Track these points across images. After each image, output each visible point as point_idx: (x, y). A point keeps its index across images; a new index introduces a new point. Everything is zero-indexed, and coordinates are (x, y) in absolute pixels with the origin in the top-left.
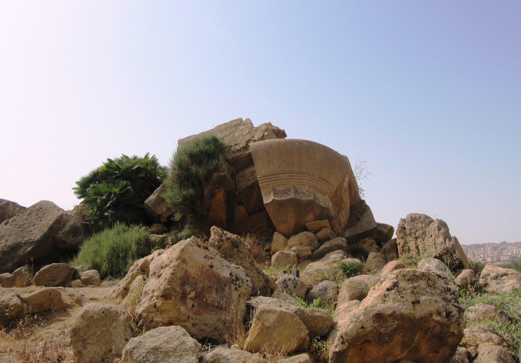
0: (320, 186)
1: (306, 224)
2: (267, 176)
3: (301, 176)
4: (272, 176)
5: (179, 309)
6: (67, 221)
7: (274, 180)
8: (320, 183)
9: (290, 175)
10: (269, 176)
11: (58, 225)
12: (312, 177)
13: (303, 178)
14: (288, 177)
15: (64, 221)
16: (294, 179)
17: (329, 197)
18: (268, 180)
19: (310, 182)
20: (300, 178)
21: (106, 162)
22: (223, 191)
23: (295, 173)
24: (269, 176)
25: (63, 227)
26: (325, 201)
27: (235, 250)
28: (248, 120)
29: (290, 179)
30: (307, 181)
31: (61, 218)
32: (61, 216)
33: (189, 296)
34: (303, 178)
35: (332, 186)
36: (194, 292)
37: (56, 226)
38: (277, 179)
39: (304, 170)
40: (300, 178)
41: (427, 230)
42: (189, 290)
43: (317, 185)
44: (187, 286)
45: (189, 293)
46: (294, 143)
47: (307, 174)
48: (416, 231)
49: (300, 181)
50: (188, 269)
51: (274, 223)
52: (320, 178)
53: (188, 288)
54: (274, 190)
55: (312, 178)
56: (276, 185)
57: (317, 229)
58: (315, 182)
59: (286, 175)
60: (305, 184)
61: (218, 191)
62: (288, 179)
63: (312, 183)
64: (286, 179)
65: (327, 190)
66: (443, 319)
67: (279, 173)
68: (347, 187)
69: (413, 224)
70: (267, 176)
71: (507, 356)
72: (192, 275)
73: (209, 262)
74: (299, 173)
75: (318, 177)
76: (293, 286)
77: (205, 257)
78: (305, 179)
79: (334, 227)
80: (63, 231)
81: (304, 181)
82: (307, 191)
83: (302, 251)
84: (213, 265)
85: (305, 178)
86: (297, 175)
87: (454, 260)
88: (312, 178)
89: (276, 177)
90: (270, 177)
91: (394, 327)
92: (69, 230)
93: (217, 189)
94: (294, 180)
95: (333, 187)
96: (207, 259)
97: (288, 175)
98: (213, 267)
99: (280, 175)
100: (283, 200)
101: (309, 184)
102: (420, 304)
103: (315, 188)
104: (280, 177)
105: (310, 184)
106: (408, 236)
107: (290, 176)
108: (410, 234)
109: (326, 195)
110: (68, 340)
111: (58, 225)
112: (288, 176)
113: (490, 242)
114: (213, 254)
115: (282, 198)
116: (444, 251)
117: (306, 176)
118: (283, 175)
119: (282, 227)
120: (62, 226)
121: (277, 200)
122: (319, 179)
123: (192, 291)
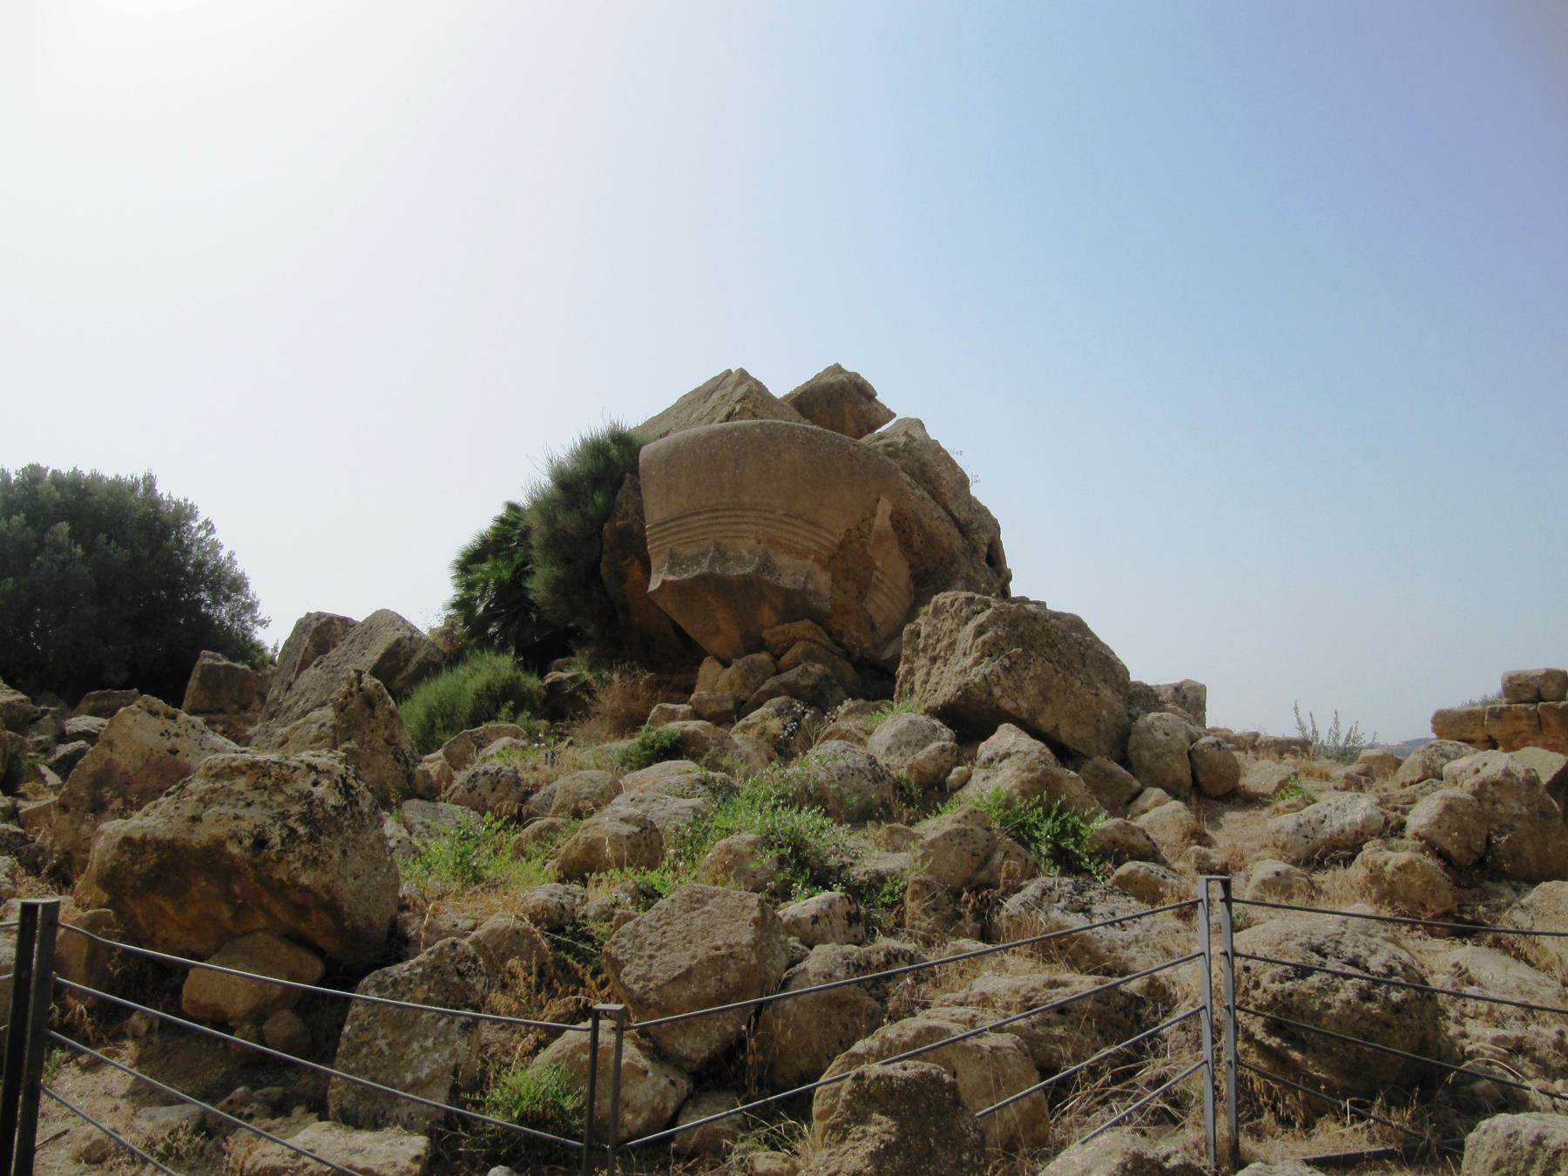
1: (765, 634)
2: (673, 520)
3: (736, 516)
4: (673, 524)
5: (78, 829)
6: (414, 651)
7: (675, 533)
8: (790, 528)
9: (712, 515)
10: (666, 522)
11: (394, 662)
12: (767, 515)
13: (741, 520)
14: (706, 522)
15: (406, 653)
16: (720, 524)
17: (818, 560)
18: (666, 533)
19: (761, 527)
20: (733, 520)
21: (500, 511)
22: (636, 563)
23: (724, 510)
24: (666, 522)
25: (406, 665)
26: (791, 571)
27: (368, 711)
29: (712, 525)
31: (399, 645)
32: (398, 643)
33: (111, 807)
34: (741, 520)
35: (827, 530)
36: (120, 799)
37: (387, 664)
39: (746, 499)
40: (733, 520)
41: (960, 636)
42: (109, 795)
44: (105, 789)
45: (110, 802)
46: (728, 433)
47: (752, 509)
48: (938, 641)
49: (734, 527)
50: (116, 757)
51: (695, 636)
53: (107, 792)
54: (671, 558)
55: (765, 519)
56: (679, 545)
57: (785, 644)
58: (773, 527)
59: (702, 517)
60: (743, 534)
61: (628, 565)
62: (707, 526)
63: (766, 529)
64: (702, 526)
68: (890, 529)
69: (934, 621)
70: (673, 520)
72: (123, 766)
73: (168, 745)
74: (733, 509)
75: (781, 512)
76: (489, 787)
77: (162, 735)
78: (746, 523)
79: (841, 635)
80: (405, 674)
81: (744, 526)
82: (750, 552)
83: (707, 702)
84: (179, 748)
85: (746, 520)
86: (727, 513)
88: (765, 519)
89: (679, 526)
90: (668, 525)
91: (152, 862)
92: (414, 672)
93: (624, 559)
95: (833, 534)
96: (167, 737)
97: (707, 515)
98: (178, 751)
99: (689, 519)
100: (684, 580)
103: (772, 541)
106: (921, 654)
107: (712, 518)
108: (925, 650)
109: (806, 558)
111: (394, 662)
112: (708, 519)
114: (184, 727)
115: (685, 576)
116: (960, 693)
117: (749, 513)
118: (696, 518)
119: (716, 644)
120: (402, 664)
121: (671, 581)
122: (787, 520)
123: (116, 798)
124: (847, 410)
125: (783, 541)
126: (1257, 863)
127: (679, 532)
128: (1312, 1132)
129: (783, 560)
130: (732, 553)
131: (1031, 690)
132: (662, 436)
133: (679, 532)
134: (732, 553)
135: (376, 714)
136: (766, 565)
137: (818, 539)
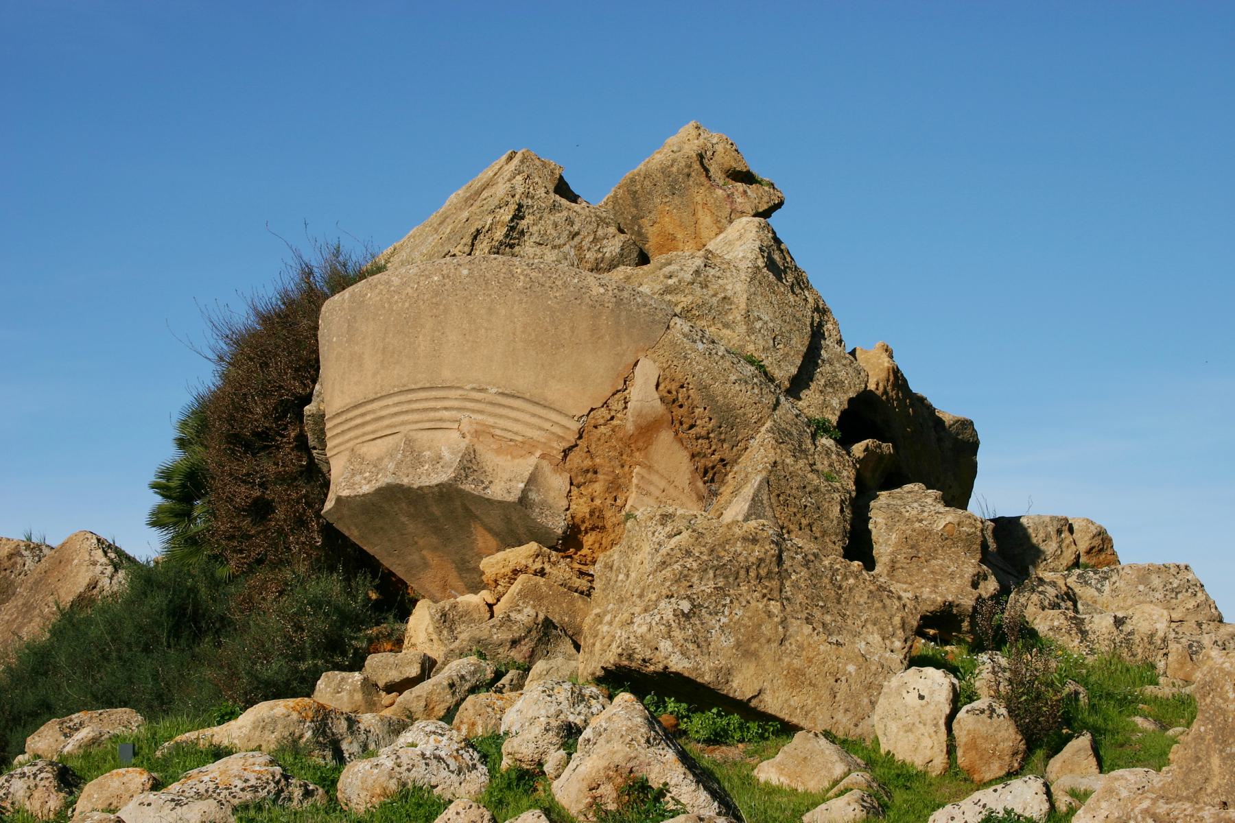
0: (502, 423)
7: (357, 426)
9: (402, 398)
28: (967, 424)
30: (454, 413)
38: (368, 418)
43: (490, 421)
52: (503, 394)
63: (473, 416)
65: (530, 433)
66: (464, 619)
67: (374, 396)
71: (319, 778)
75: (494, 390)
78: (446, 409)
81: (446, 414)
87: (824, 495)
94: (415, 417)
97: (396, 399)
99: (375, 405)
101: (459, 421)
102: (48, 774)
104: (373, 411)
105: (465, 421)
110: (834, 419)
113: (1150, 562)
124: (884, 445)
125: (498, 432)
126: (53, 546)
127: (363, 424)
128: (151, 782)
129: (490, 458)
130: (427, 453)
131: (723, 642)
132: (502, 429)
133: (363, 424)
134: (427, 453)
135: (1052, 761)
136: (469, 464)
137: (547, 425)
